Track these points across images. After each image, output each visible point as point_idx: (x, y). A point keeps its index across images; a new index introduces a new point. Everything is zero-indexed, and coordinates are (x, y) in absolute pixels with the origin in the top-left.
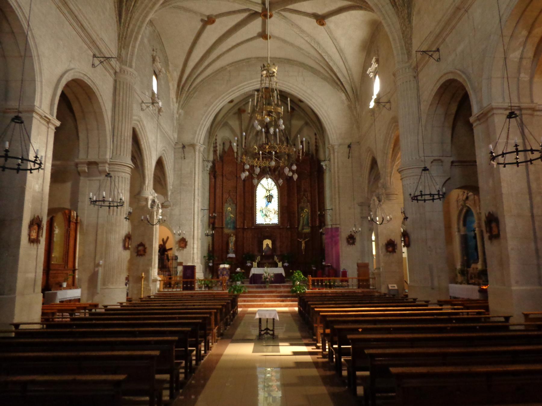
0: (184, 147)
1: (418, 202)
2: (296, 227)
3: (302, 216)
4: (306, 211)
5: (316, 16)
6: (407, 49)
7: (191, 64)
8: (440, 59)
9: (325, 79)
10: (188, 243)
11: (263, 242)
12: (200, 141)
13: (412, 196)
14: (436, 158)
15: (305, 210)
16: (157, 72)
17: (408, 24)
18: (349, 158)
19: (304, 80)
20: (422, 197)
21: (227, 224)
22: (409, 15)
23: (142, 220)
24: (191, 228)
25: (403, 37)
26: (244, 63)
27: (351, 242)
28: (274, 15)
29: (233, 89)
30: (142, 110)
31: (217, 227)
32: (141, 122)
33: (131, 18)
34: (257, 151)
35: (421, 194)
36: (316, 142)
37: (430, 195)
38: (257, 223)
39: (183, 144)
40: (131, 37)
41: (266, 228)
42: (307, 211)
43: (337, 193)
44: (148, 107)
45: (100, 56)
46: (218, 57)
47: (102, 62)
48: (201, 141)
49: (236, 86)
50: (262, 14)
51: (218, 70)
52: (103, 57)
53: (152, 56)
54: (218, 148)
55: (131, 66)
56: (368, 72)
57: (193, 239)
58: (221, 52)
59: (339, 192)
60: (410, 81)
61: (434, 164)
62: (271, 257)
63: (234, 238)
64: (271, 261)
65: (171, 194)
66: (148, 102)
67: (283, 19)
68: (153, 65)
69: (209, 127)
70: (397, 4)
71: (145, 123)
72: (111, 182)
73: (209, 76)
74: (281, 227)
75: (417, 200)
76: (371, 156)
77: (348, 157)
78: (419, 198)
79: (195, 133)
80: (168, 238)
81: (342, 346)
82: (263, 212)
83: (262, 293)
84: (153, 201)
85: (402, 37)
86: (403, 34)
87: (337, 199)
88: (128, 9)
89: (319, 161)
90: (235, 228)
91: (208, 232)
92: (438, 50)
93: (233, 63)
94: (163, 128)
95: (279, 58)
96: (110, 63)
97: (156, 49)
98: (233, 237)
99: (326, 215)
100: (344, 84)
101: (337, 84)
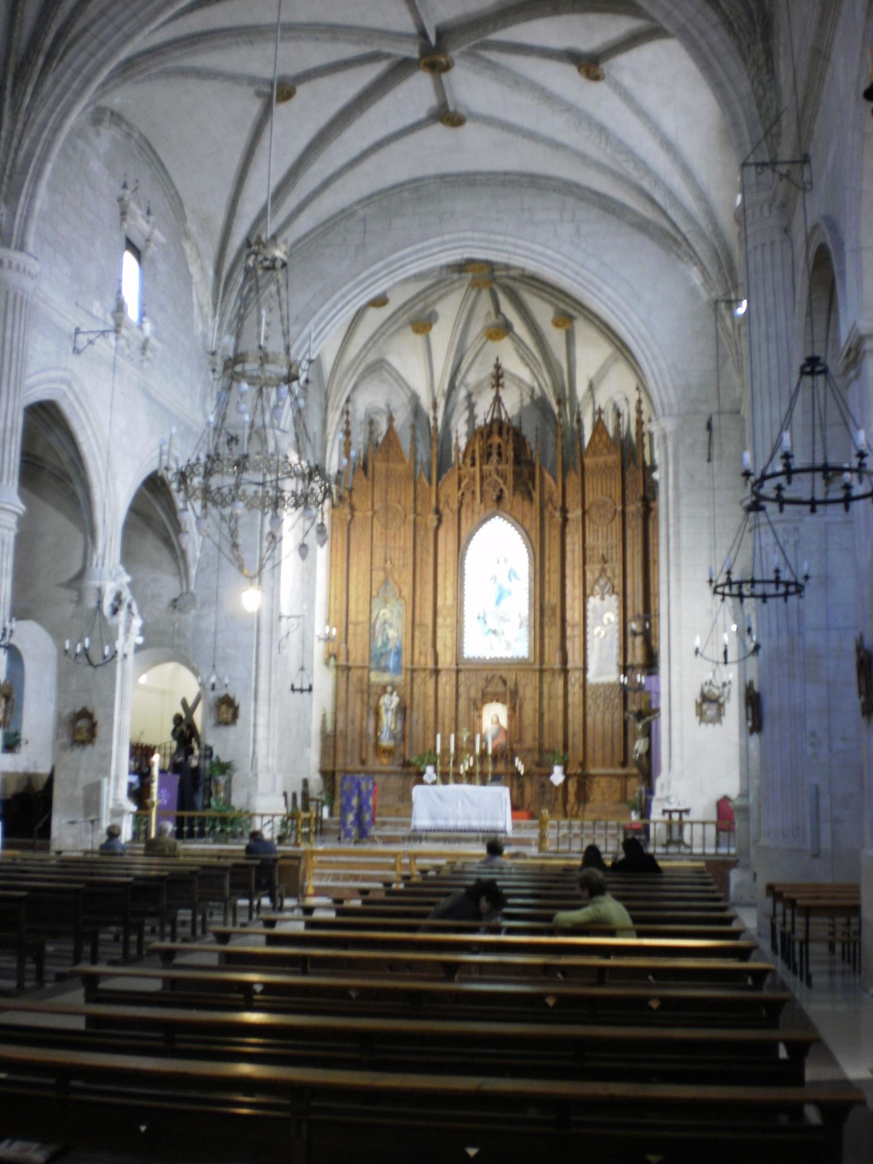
5: (573, 57)
7: (249, 210)
10: (242, 712)
16: (139, 242)
17: (770, 81)
19: (578, 232)
20: (777, 588)
22: (769, 55)
24: (250, 672)
28: (457, 61)
29: (373, 269)
30: (77, 351)
32: (75, 386)
33: (25, 124)
40: (24, 172)
44: (91, 342)
46: (326, 184)
49: (381, 259)
50: (422, 63)
51: (331, 219)
55: (21, 247)
57: (256, 699)
58: (329, 171)
60: (763, 245)
65: (197, 575)
68: (121, 224)
69: (838, 284)
70: (735, 26)
73: (305, 236)
77: (706, 457)
82: (485, 622)
84: (118, 598)
86: (759, 106)
88: (19, 103)
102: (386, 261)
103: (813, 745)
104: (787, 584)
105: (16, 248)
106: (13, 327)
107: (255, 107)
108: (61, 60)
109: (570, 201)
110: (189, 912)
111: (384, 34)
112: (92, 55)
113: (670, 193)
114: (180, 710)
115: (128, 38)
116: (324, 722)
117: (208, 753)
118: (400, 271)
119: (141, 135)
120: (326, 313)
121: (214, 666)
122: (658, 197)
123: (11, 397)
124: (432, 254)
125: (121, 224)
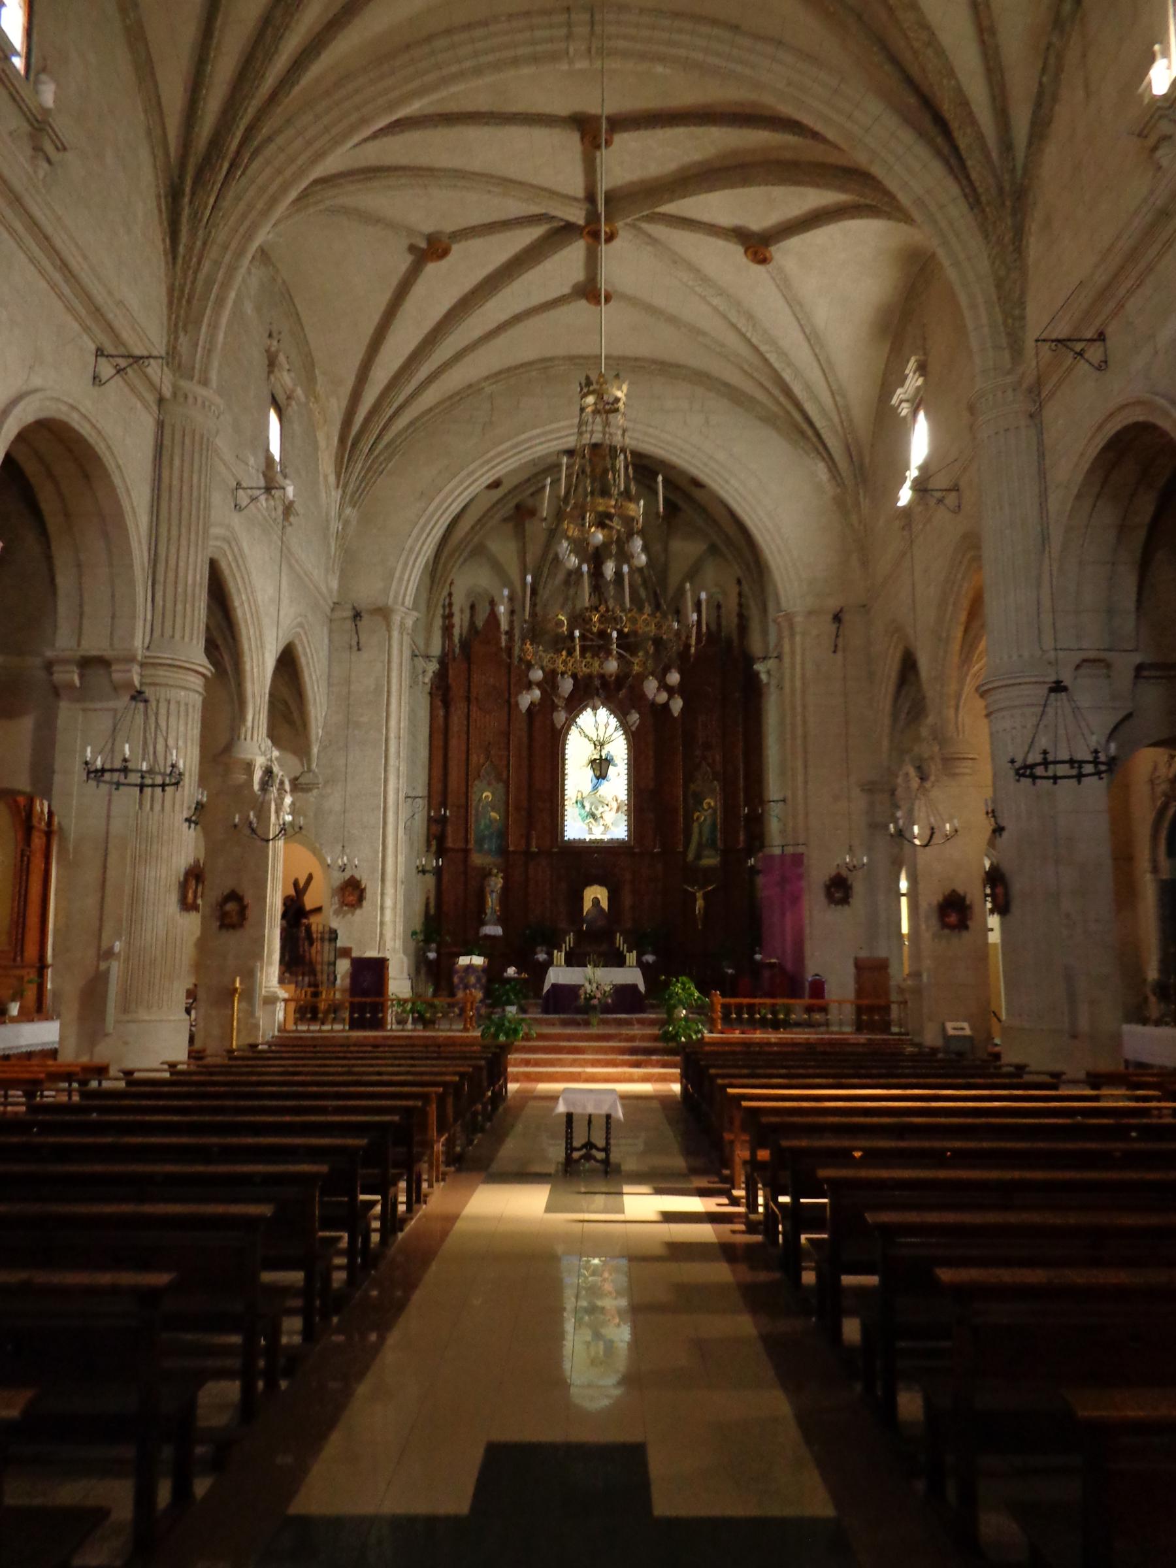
0: (357, 615)
1: (1034, 784)
2: (681, 849)
3: (698, 818)
4: (709, 804)
5: (741, 236)
7: (380, 376)
9: (769, 420)
10: (368, 894)
13: (1017, 765)
14: (1091, 655)
16: (281, 398)
18: (835, 652)
19: (707, 422)
21: (480, 841)
22: (1019, 233)
25: (999, 299)
27: (838, 895)
34: (565, 628)
35: (1045, 759)
36: (740, 605)
39: (354, 608)
40: (205, 297)
42: (712, 804)
45: (113, 352)
49: (509, 439)
53: (267, 351)
54: (456, 620)
55: (205, 382)
56: (894, 401)
57: (383, 880)
61: (1082, 671)
63: (502, 881)
68: (268, 378)
71: (245, 546)
75: (1034, 777)
76: (901, 647)
77: (833, 649)
78: (1039, 771)
80: (310, 878)
82: (584, 807)
85: (995, 298)
89: (748, 660)
90: (503, 852)
92: (1101, 337)
93: (500, 372)
94: (297, 561)
95: (636, 359)
98: (496, 876)
101: (802, 433)
102: (515, 441)
105: (199, 382)
106: (200, 471)
107: (404, 262)
108: (243, 173)
110: (759, 1158)
111: (553, 194)
112: (279, 172)
114: (292, 892)
115: (320, 156)
116: (427, 905)
117: (333, 936)
119: (284, 282)
120: (452, 491)
123: (200, 548)
125: (268, 378)
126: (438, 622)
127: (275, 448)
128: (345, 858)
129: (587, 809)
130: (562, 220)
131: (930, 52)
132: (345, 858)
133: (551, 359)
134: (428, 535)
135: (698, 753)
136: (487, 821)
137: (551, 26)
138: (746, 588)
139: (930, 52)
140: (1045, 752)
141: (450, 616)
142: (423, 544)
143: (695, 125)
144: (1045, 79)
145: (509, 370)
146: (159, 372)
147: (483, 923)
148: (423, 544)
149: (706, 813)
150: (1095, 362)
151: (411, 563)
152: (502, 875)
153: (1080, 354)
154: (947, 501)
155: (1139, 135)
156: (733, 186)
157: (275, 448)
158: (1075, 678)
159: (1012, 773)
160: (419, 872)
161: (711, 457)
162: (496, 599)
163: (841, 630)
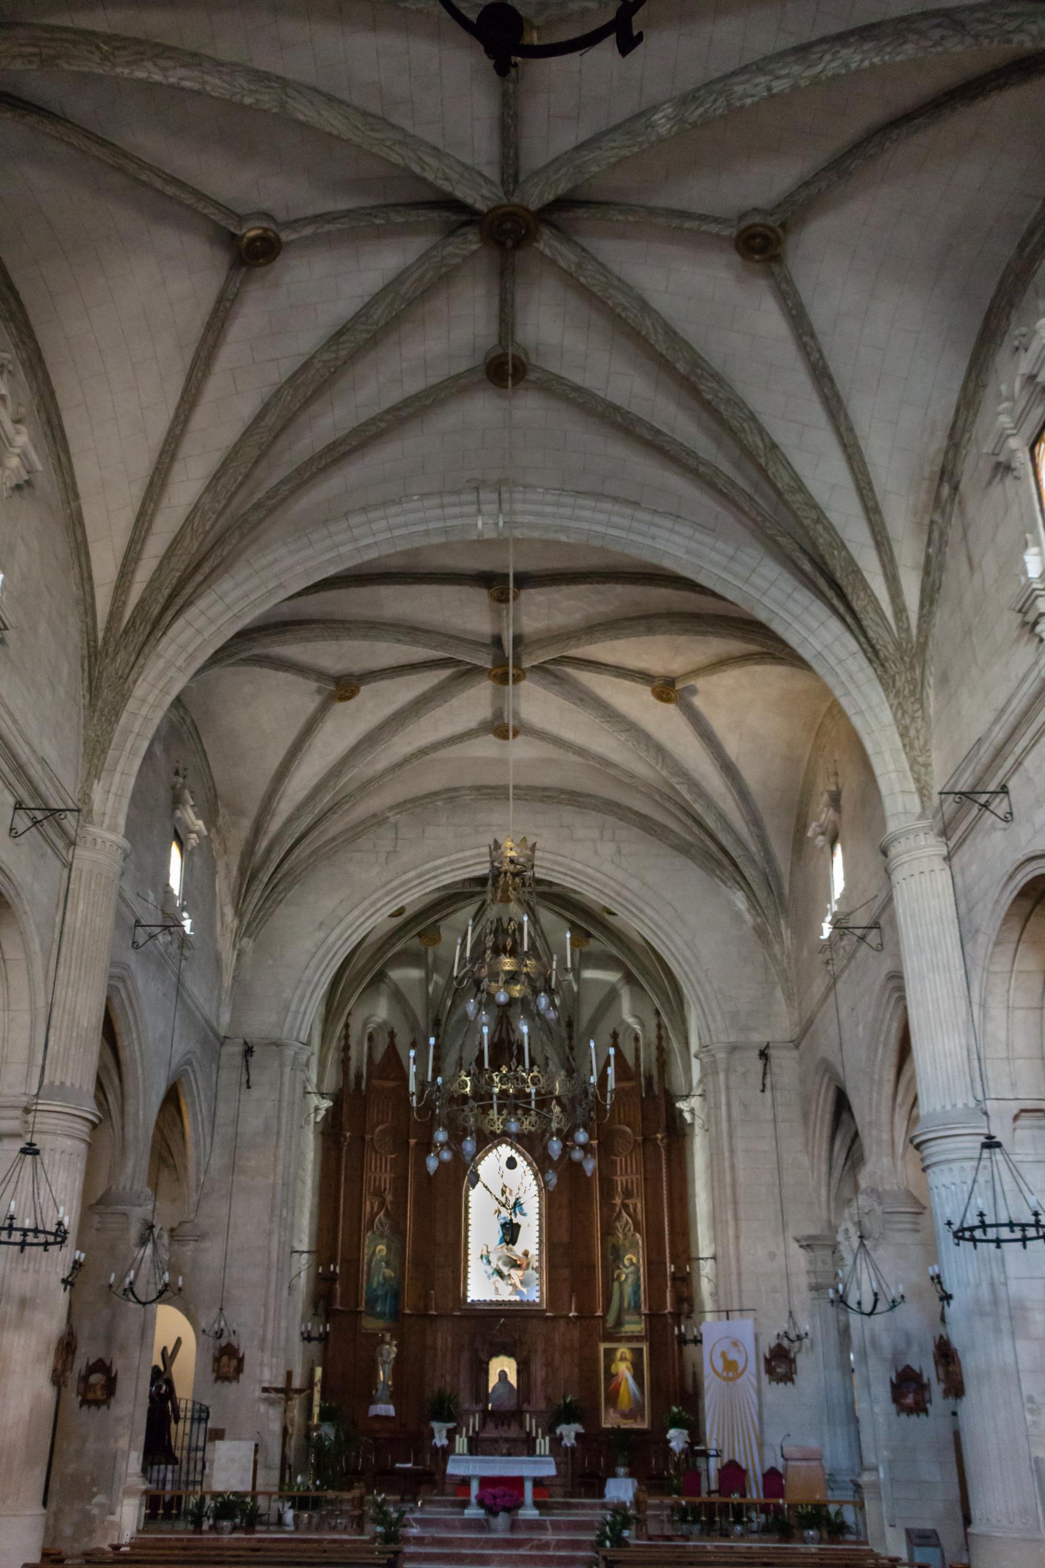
0: (248, 1051)
1: (975, 1247)
2: (599, 1313)
3: (619, 1276)
4: (631, 1260)
6: (917, 780)
8: (1011, 814)
9: (684, 849)
11: (487, 1364)
12: (299, 1033)
13: (955, 1227)
14: (1029, 1105)
15: (628, 1256)
18: (763, 1091)
19: (619, 851)
21: (371, 1302)
23: (110, 1286)
25: (904, 746)
26: (439, 803)
27: (780, 1371)
31: (337, 1310)
32: (129, 982)
34: (468, 1089)
35: (982, 1222)
36: (660, 1038)
37: (1011, 1225)
38: (469, 1300)
39: (246, 1043)
41: (500, 1317)
42: (634, 1260)
43: (730, 1206)
44: (152, 937)
45: (33, 806)
47: (38, 822)
48: (302, 1033)
49: (416, 868)
52: (42, 809)
53: (173, 788)
54: (353, 1053)
56: (810, 834)
59: (735, 1203)
61: (1020, 1122)
62: (515, 1415)
63: (395, 1349)
64: (513, 1432)
66: (153, 923)
67: (555, 684)
71: (140, 984)
72: (35, 1168)
74: (548, 1314)
75: (973, 1240)
76: (832, 1088)
77: (760, 1087)
78: (978, 1234)
79: (287, 1008)
80: (179, 1342)
81: (398, 1465)
82: (489, 1262)
83: (482, 1547)
85: (900, 745)
86: (902, 735)
87: (731, 1223)
89: (670, 1098)
90: (396, 1314)
91: (309, 1328)
92: (1004, 790)
93: (405, 802)
94: (189, 996)
95: (544, 789)
96: (59, 824)
97: (185, 769)
98: (389, 1344)
99: (694, 1274)
100: (741, 866)
101: (719, 864)
102: (419, 870)
103: (1032, 1411)
104: (25, 1232)
109: (611, 819)
113: (722, 817)
118: (433, 881)
121: (221, 1309)
122: (710, 821)
124: (467, 866)
126: (332, 1056)
127: (175, 882)
128: (222, 1323)
129: (494, 1265)
130: (469, 663)
131: (820, 528)
132: (222, 1323)
133: (456, 789)
134: (327, 966)
135: (618, 1201)
136: (381, 1278)
137: (460, 504)
138: (665, 1019)
139: (820, 528)
140: (981, 1215)
141: (346, 1048)
142: (322, 975)
143: (598, 583)
144: (931, 550)
145: (413, 800)
146: (74, 824)
147: (373, 1401)
148: (322, 975)
149: (627, 1271)
150: (1001, 814)
151: (308, 995)
152: (395, 1342)
153: (985, 806)
154: (868, 939)
155: (1020, 611)
156: (639, 634)
157: (175, 882)
158: (1015, 1129)
159: (951, 1235)
160: (304, 1339)
161: (624, 886)
162: (396, 1031)
163: (768, 1067)
